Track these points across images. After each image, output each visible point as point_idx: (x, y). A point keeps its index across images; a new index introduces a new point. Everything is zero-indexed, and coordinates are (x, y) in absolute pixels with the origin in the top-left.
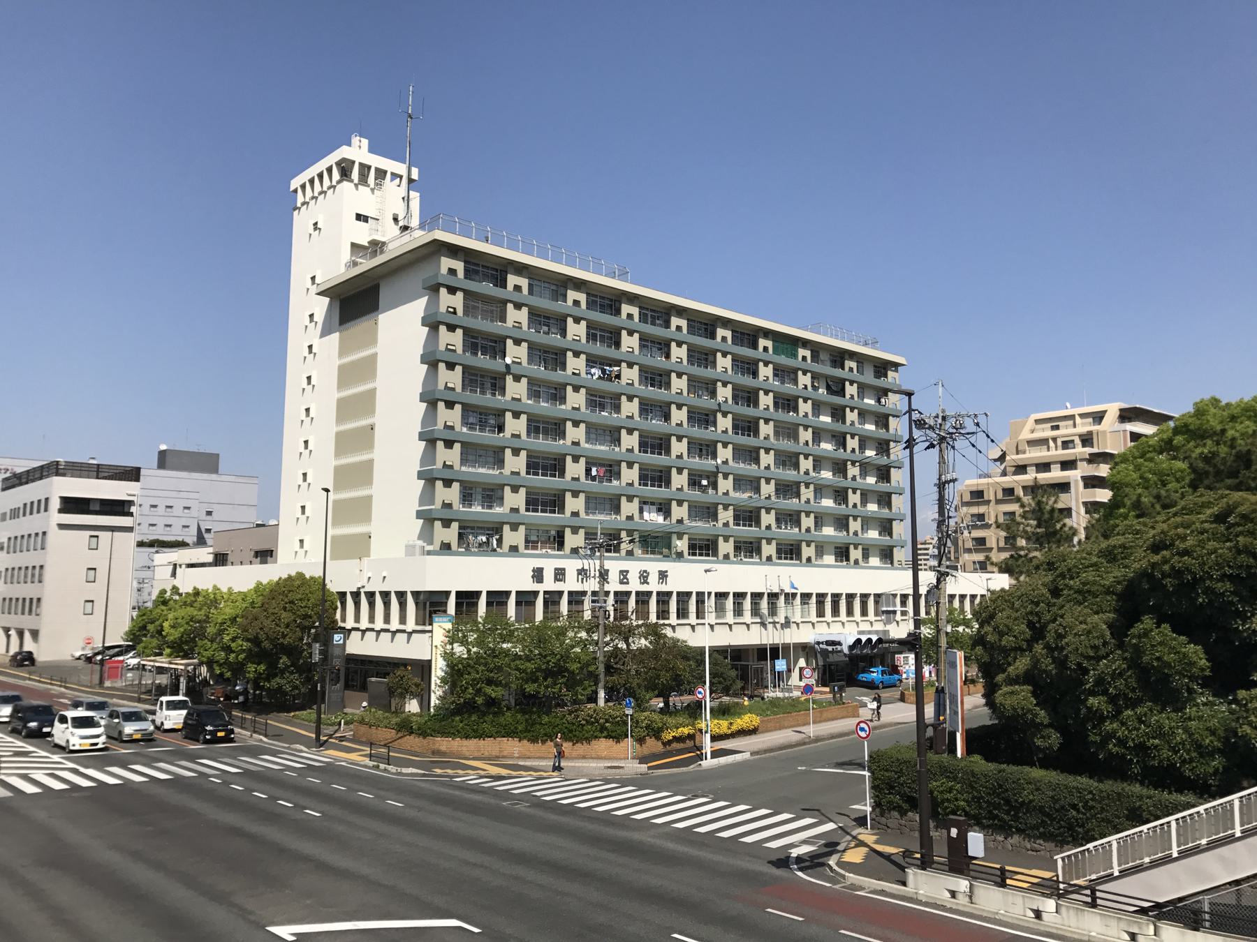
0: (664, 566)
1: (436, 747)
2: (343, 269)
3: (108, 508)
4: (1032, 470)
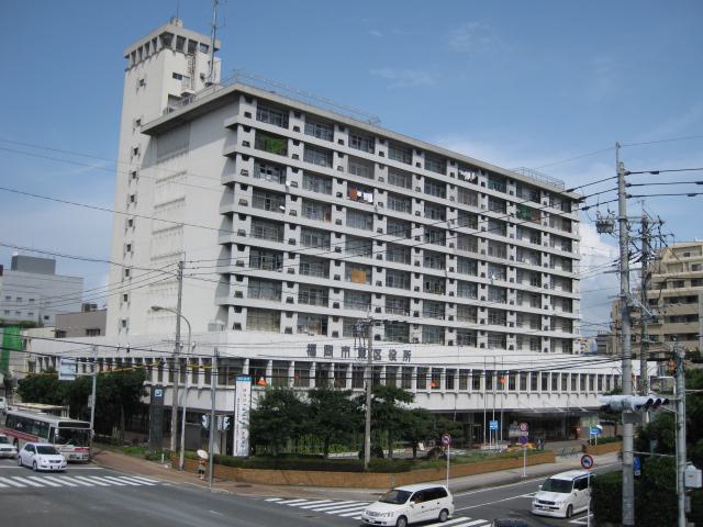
0: (407, 347)
1: (239, 475)
2: (161, 115)
4: (687, 283)
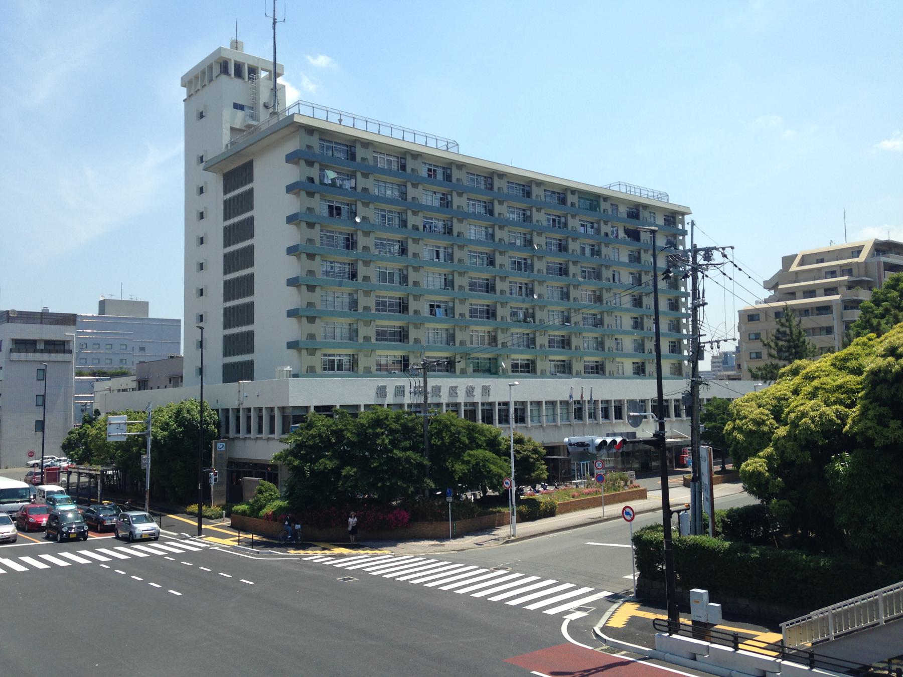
3: (51, 347)
